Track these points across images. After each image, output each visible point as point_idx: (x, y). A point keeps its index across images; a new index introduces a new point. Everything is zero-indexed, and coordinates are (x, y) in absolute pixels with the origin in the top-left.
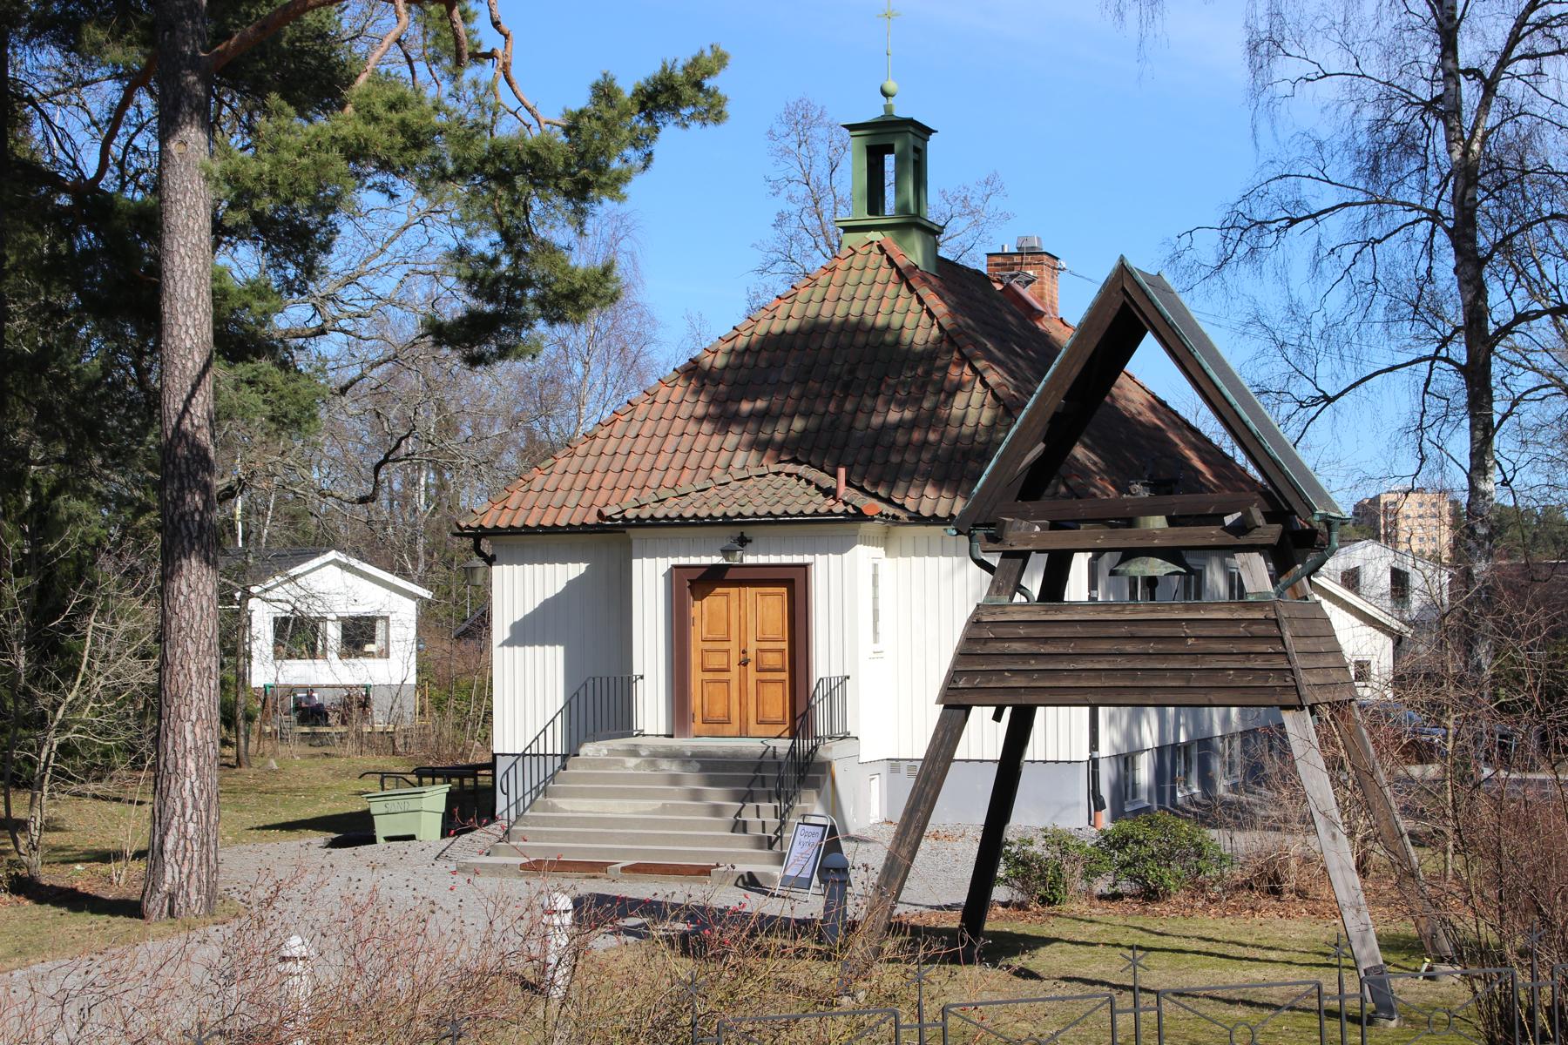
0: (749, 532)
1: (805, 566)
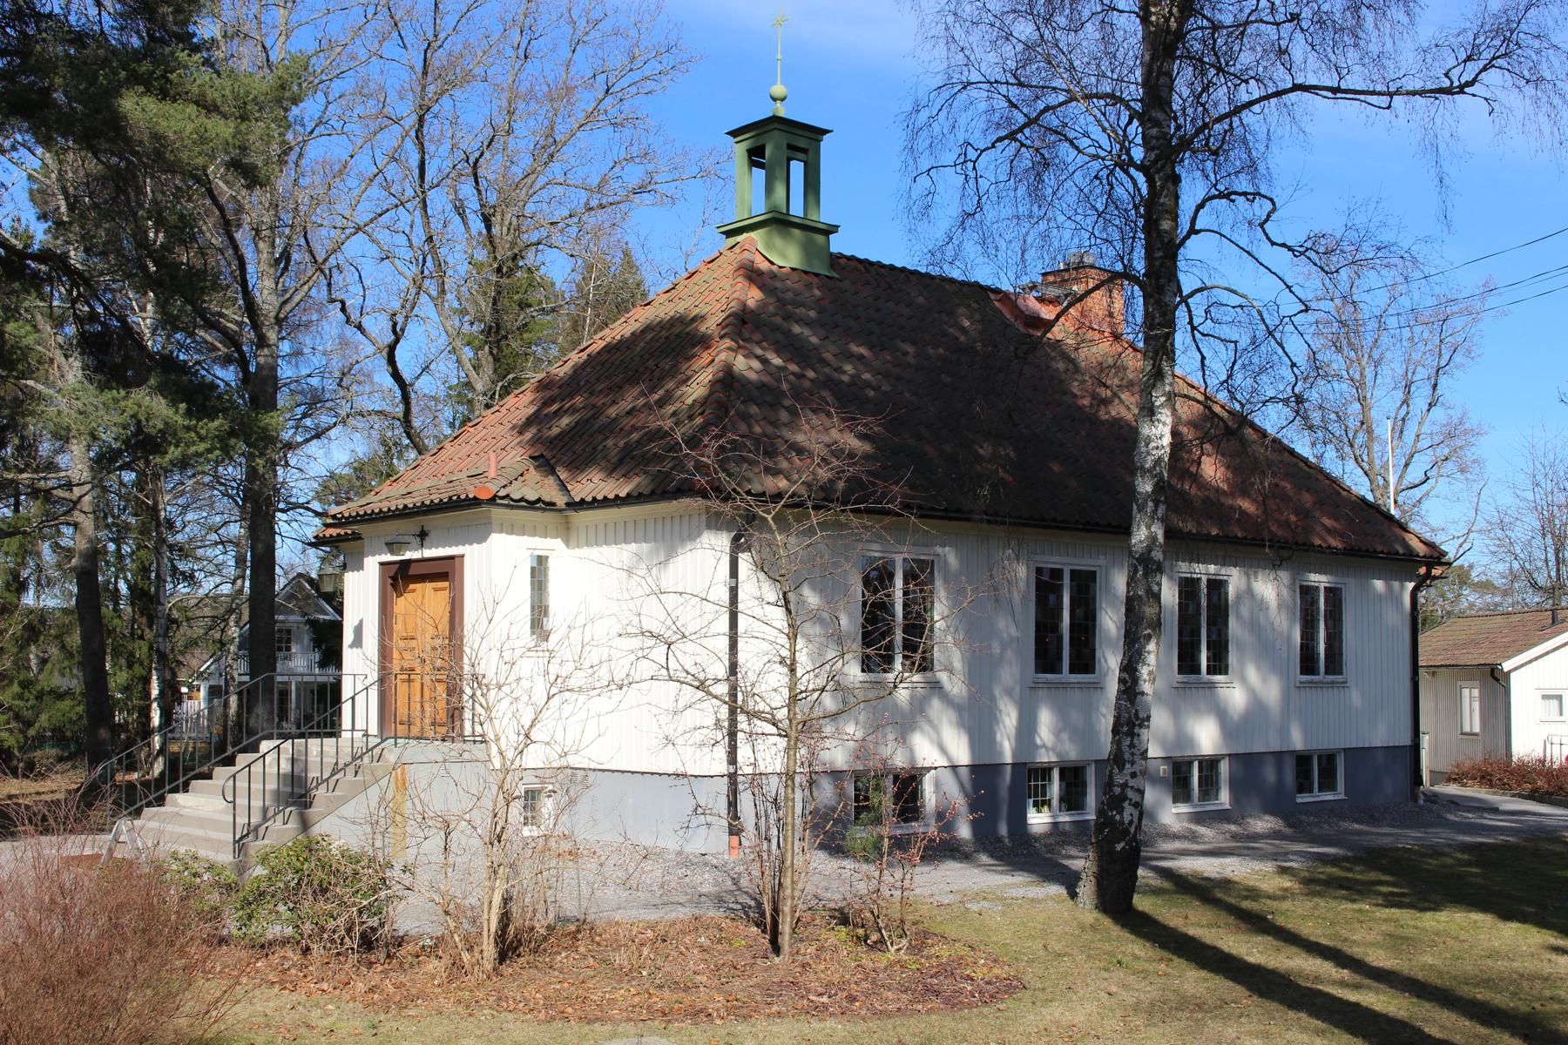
0: (430, 521)
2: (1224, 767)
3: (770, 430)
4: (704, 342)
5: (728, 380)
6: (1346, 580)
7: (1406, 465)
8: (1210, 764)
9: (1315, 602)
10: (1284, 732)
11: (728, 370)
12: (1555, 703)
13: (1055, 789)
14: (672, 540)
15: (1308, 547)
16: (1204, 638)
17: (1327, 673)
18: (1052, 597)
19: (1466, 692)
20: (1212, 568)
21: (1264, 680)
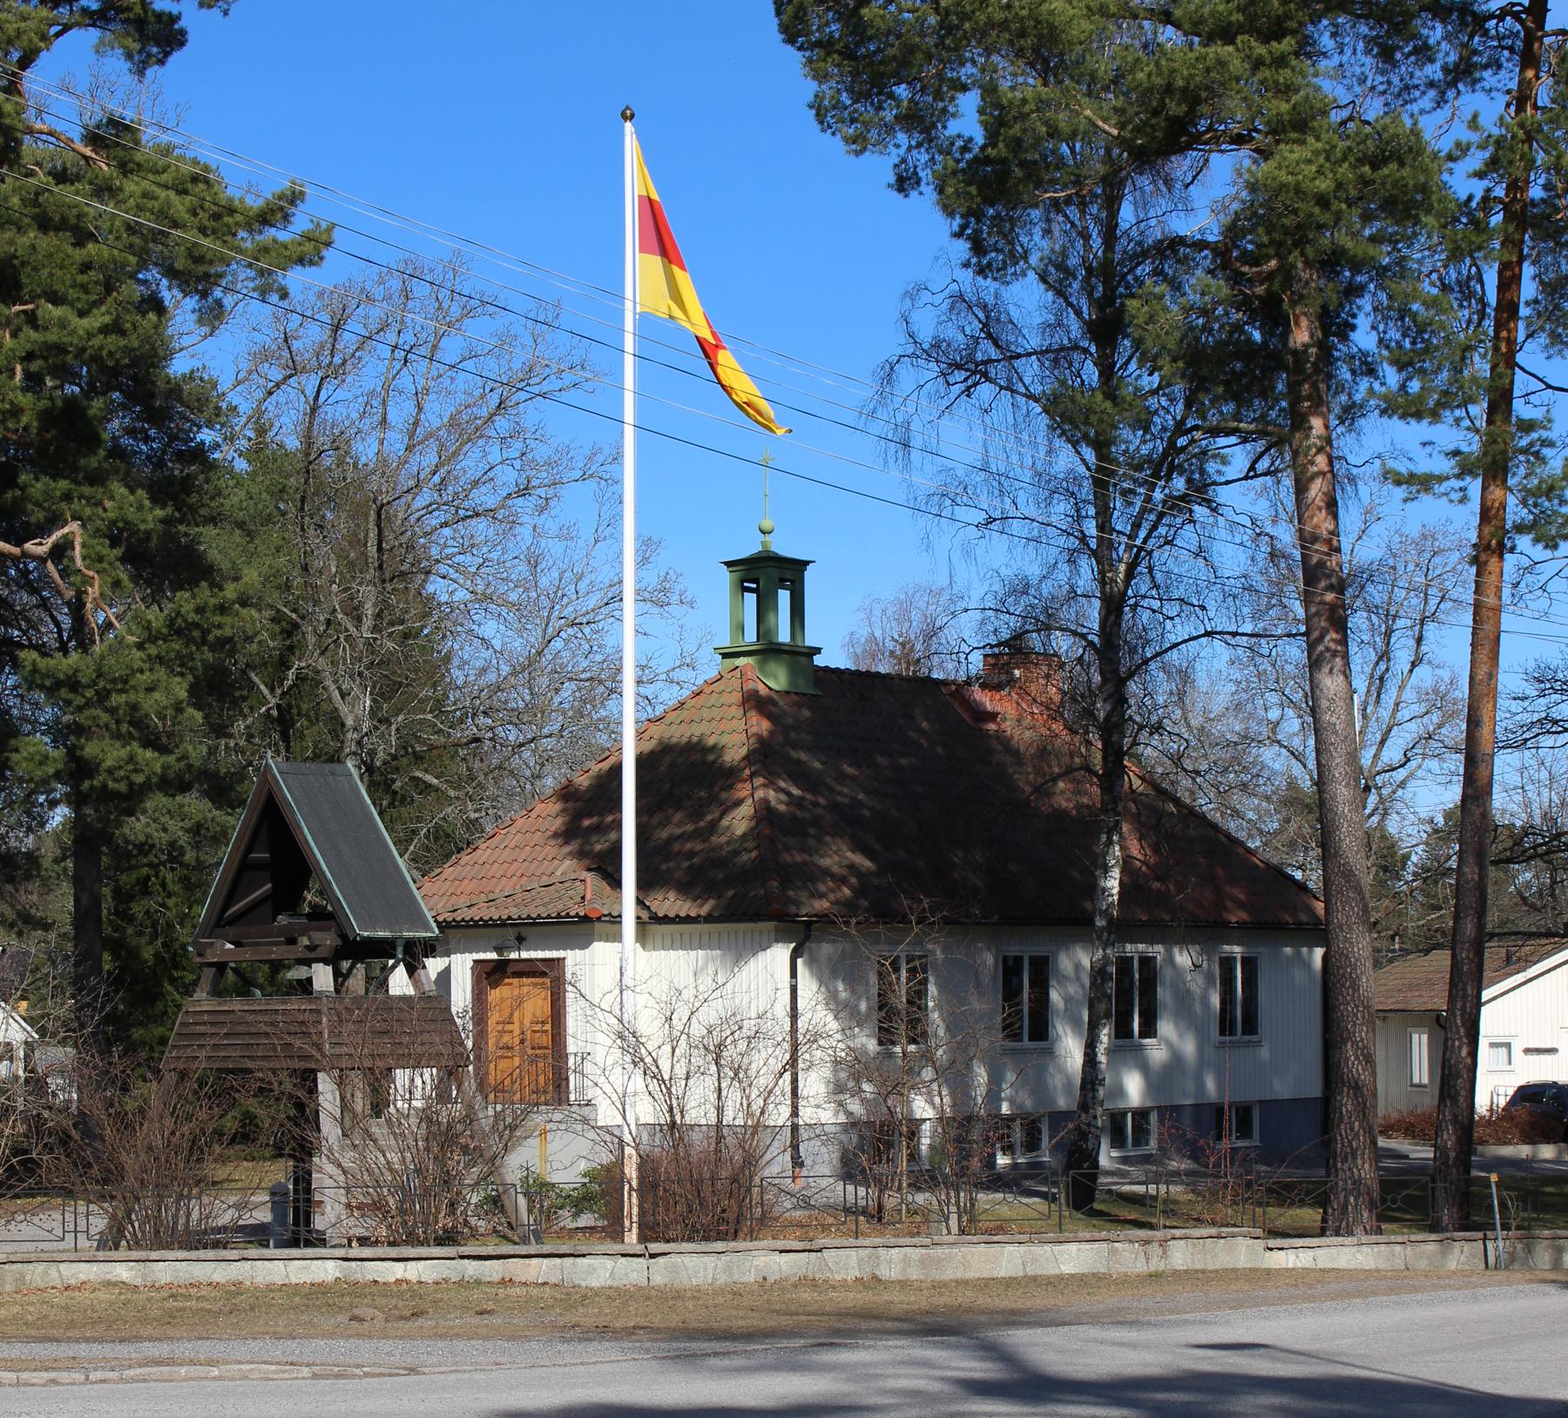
0: (524, 931)
2: (1154, 1118)
3: (806, 857)
4: (730, 775)
5: (765, 814)
6: (1262, 949)
7: (1383, 742)
9: (1232, 970)
10: (1200, 1085)
11: (766, 801)
12: (1504, 1051)
13: (1018, 1135)
14: (740, 952)
15: (1225, 925)
17: (1244, 1033)
18: (1015, 980)
19: (1415, 1037)
20: (1141, 947)
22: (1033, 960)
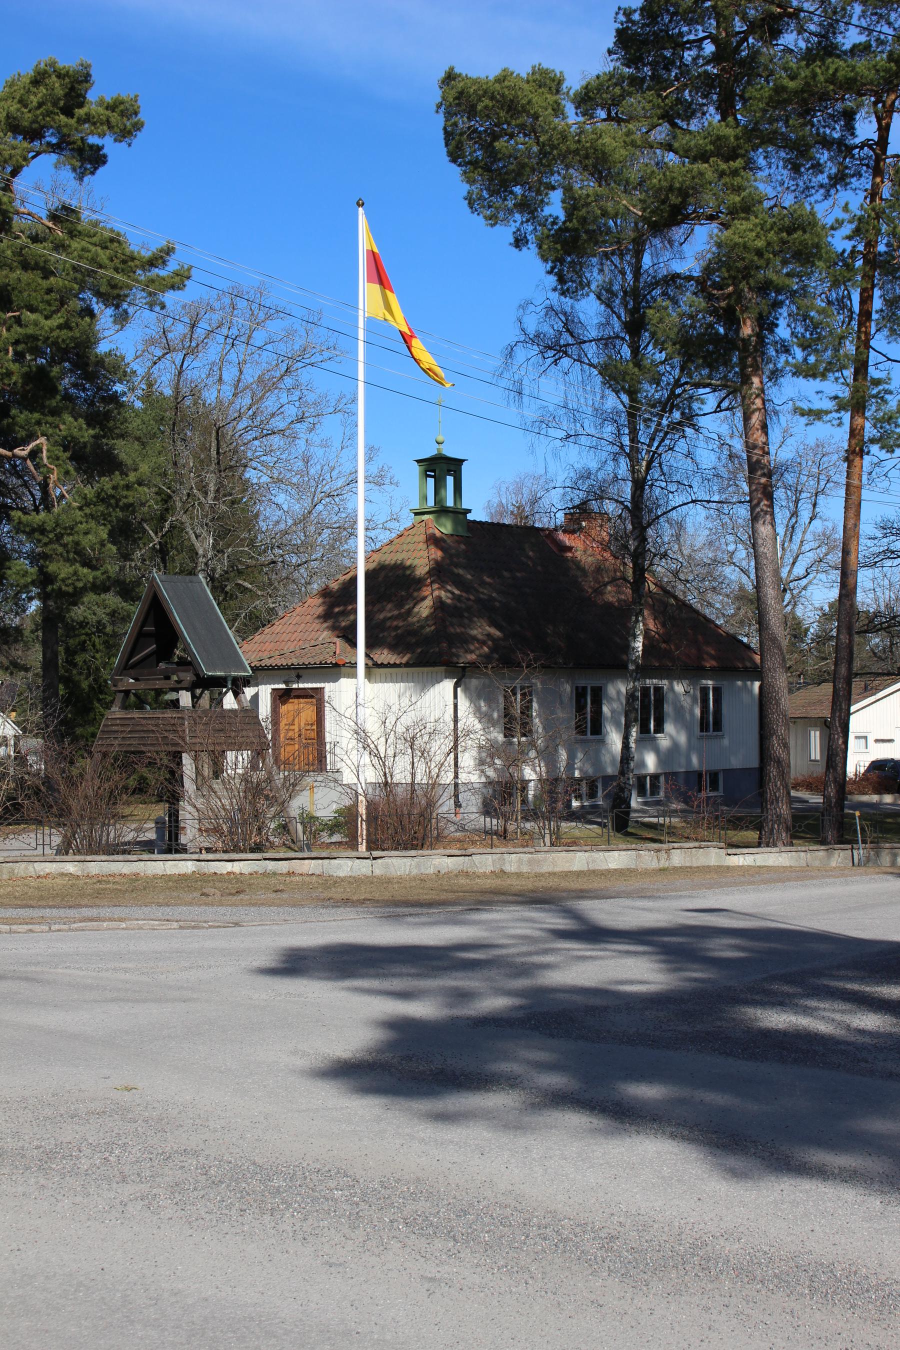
0: (301, 672)
1: (321, 690)
2: (662, 779)
4: (419, 583)
5: (439, 605)
7: (794, 563)
8: (655, 777)
9: (707, 695)
10: (689, 760)
11: (439, 597)
13: (584, 789)
14: (425, 684)
15: (703, 668)
16: (647, 713)
19: (812, 733)
20: (655, 681)
21: (678, 732)
22: (593, 689)
